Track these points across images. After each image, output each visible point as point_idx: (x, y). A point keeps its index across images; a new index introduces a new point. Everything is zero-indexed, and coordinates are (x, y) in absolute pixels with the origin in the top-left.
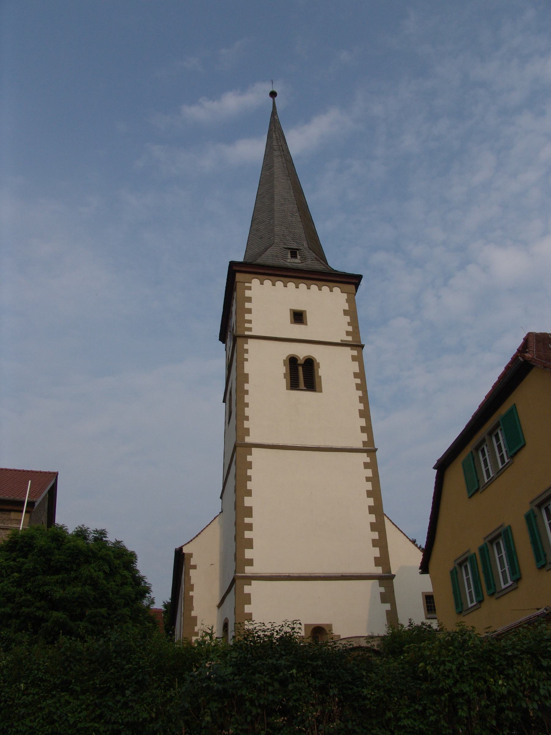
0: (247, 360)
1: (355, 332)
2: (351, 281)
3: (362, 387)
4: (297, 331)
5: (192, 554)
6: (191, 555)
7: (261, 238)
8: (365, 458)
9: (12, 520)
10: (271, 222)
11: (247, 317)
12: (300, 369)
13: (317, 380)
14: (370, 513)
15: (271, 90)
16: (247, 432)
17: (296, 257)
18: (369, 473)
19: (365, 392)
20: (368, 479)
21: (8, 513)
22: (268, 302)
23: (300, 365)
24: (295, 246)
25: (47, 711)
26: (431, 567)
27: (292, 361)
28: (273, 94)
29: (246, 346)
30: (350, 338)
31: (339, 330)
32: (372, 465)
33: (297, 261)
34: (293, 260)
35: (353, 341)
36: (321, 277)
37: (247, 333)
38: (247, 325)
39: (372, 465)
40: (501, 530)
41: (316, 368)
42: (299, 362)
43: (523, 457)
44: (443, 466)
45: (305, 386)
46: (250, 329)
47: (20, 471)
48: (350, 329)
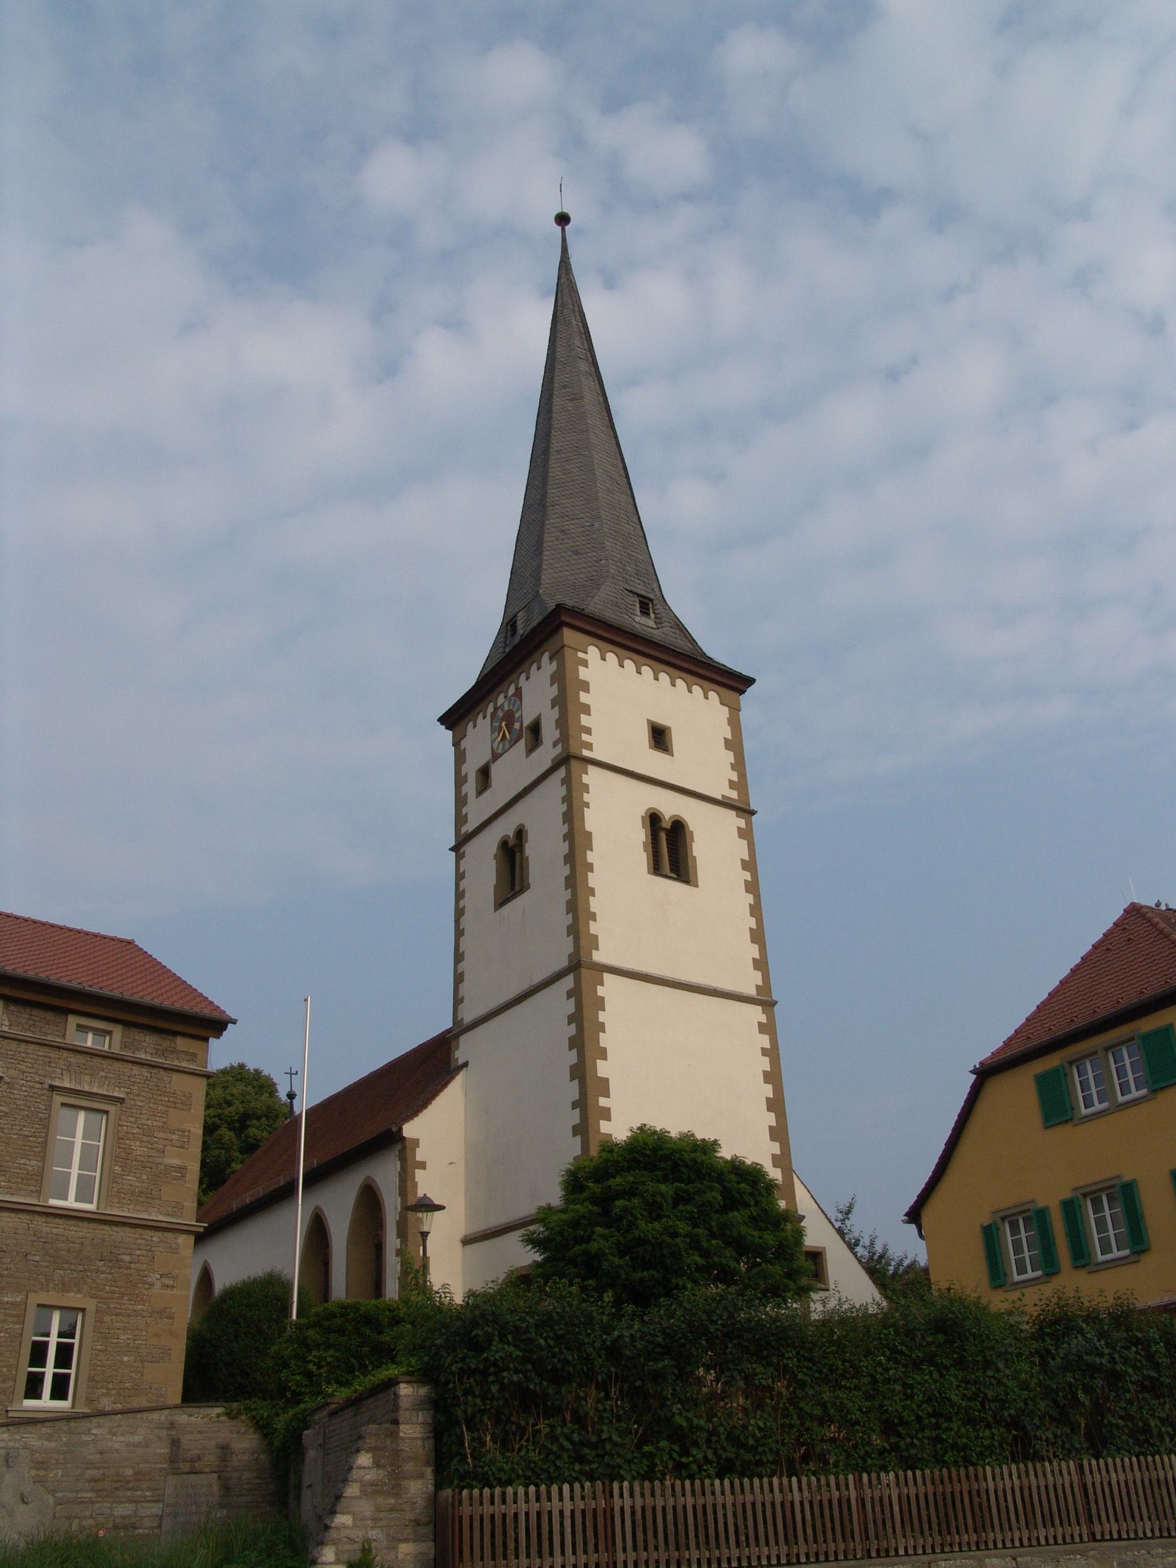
1: (740, 785)
3: (752, 887)
5: (418, 1140)
6: (416, 1143)
7: (577, 553)
8: (756, 1014)
9: (179, 1052)
10: (596, 525)
11: (585, 720)
12: (663, 836)
16: (594, 942)
18: (765, 1041)
19: (757, 897)
20: (765, 1052)
21: (170, 1037)
22: (616, 695)
26: (927, 1216)
27: (654, 819)
29: (586, 779)
30: (734, 795)
31: (716, 777)
34: (644, 620)
36: (719, 678)
37: (586, 753)
38: (585, 737)
39: (768, 1028)
40: (1030, 1206)
44: (986, 1074)
45: (672, 870)
46: (589, 746)
47: (44, 924)
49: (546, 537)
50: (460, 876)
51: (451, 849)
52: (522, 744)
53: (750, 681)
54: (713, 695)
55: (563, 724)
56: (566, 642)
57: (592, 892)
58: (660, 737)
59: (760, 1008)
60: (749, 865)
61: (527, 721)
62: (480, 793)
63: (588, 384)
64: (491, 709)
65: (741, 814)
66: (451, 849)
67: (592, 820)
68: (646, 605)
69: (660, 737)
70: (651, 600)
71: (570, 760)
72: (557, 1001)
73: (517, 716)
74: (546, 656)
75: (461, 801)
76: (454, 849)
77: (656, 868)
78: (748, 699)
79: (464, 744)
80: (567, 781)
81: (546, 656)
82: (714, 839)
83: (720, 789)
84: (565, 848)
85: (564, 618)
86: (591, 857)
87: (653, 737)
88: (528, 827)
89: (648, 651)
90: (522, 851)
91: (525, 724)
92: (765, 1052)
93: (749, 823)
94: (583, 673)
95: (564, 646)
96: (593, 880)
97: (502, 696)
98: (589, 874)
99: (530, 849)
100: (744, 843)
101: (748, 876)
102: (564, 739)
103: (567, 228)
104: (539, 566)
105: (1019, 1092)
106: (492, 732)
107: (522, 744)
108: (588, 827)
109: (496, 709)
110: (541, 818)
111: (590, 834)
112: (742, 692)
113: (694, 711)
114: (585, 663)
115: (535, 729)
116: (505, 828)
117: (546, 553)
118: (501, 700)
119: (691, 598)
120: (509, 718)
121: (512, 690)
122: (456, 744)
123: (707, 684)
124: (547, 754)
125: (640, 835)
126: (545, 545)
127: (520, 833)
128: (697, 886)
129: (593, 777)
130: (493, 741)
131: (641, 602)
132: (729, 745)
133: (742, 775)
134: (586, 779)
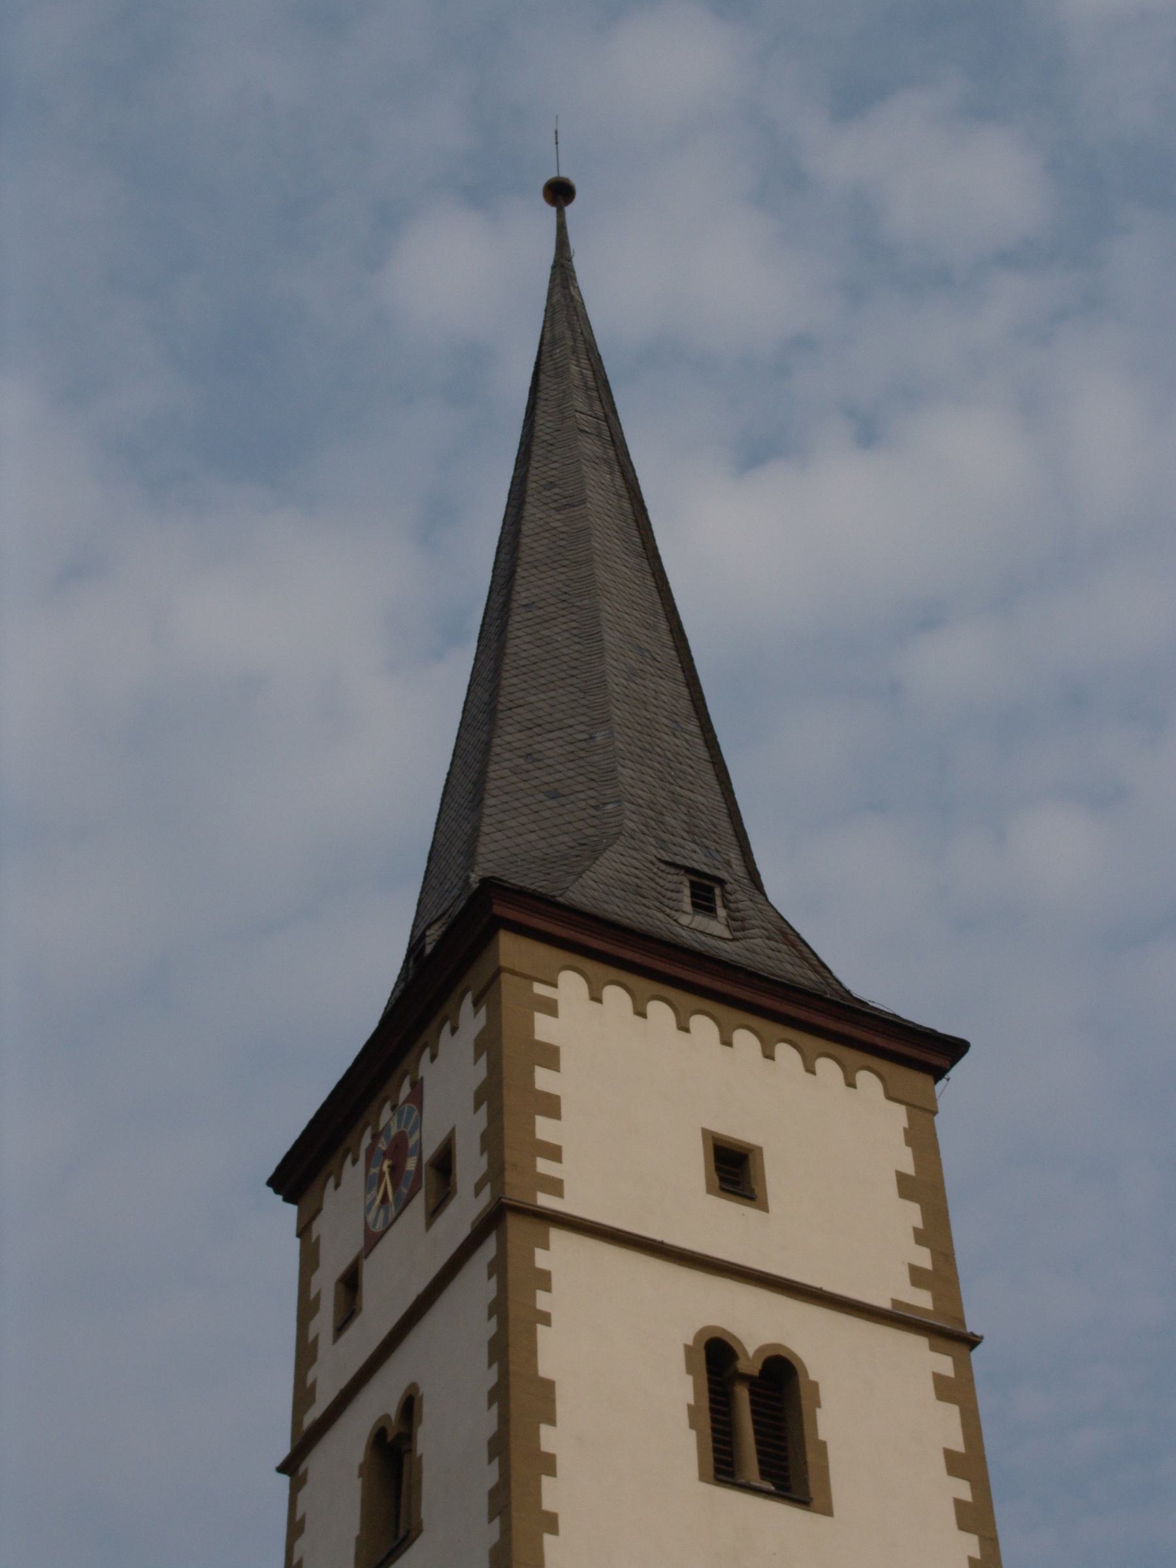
0: (546, 1319)
1: (941, 1276)
2: (917, 1054)
3: (976, 1516)
4: (721, 1227)
7: (554, 795)
10: (600, 737)
12: (743, 1394)
13: (811, 1457)
15: (551, 175)
17: (710, 911)
22: (621, 1081)
24: (699, 862)
27: (716, 1355)
28: (560, 193)
29: (542, 1259)
30: (922, 1299)
31: (884, 1267)
33: (718, 927)
37: (545, 1200)
38: (544, 1166)
41: (805, 1403)
42: (742, 1366)
45: (764, 1475)
46: (555, 1187)
48: (924, 1258)
49: (494, 770)
51: (282, 1469)
52: (418, 1204)
53: (955, 1049)
55: (493, 1141)
56: (504, 962)
57: (551, 1523)
58: (734, 1169)
60: (967, 1463)
61: (429, 1151)
62: (340, 1328)
63: (599, 484)
64: (366, 1141)
65: (940, 1342)
66: (282, 1469)
67: (555, 1354)
68: (705, 892)
69: (734, 1169)
70: (721, 882)
71: (512, 1218)
73: (412, 1142)
74: (468, 1000)
75: (306, 1354)
76: (290, 1466)
77: (723, 1468)
78: (956, 1089)
79: (319, 1227)
80: (498, 1268)
81: (468, 1000)
82: (872, 1405)
83: (889, 1286)
84: (488, 1422)
85: (498, 910)
86: (549, 1439)
87: (718, 1169)
88: (425, 1390)
89: (705, 981)
90: (411, 1450)
93: (964, 1368)
94: (544, 1028)
95: (499, 971)
96: (553, 1494)
97: (388, 1106)
98: (546, 1480)
100: (951, 1414)
101: (963, 1490)
102: (495, 1173)
103: (569, 210)
104: (476, 829)
105: (348, 1195)
106: (368, 1189)
107: (418, 1204)
108: (546, 1367)
109: (375, 1137)
110: (447, 1364)
111: (549, 1386)
112: (939, 1073)
113: (826, 1126)
114: (551, 1008)
115: (444, 1163)
116: (379, 1402)
117: (489, 801)
118: (386, 1115)
119: (837, 890)
120: (399, 1149)
121: (406, 1090)
122: (303, 1231)
123: (852, 1056)
124: (466, 1208)
125: (680, 1390)
126: (489, 786)
127: (410, 1406)
128: (827, 1511)
129: (560, 1254)
130: (368, 1209)
131: (693, 885)
132: (907, 1187)
133: (944, 1255)
134: (542, 1259)
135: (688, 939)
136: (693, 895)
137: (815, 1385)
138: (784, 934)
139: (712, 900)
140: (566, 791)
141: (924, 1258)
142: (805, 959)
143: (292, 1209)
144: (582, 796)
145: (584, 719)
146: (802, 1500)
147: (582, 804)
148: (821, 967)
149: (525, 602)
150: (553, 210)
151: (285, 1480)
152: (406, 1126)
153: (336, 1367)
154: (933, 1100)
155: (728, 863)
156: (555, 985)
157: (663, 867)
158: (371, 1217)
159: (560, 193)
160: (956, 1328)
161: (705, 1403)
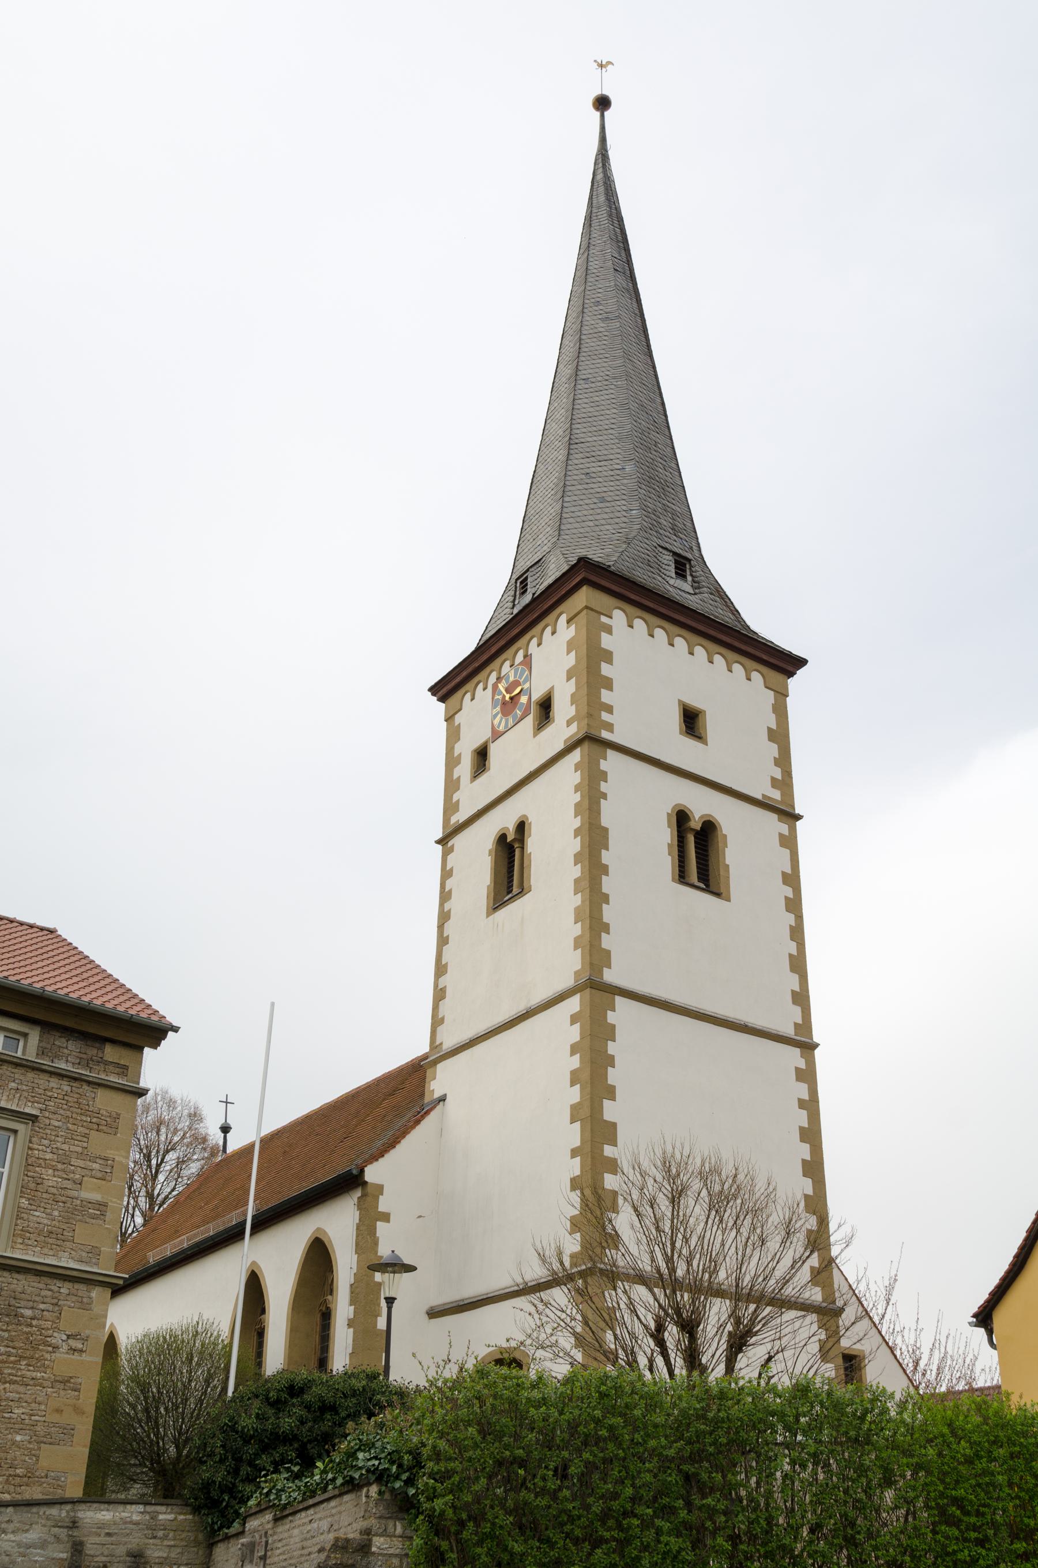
2: (784, 664)
9: (107, 1063)
12: (691, 839)
14: (614, 1125)
15: (597, 92)
20: (802, 1104)
23: (692, 829)
25: (1017, 1449)
27: (681, 817)
28: (602, 103)
30: (776, 795)
32: (807, 1075)
33: (687, 587)
34: (679, 583)
35: (782, 802)
37: (605, 735)
43: (484, 778)
45: (700, 879)
46: (610, 727)
50: (446, 874)
51: (438, 842)
54: (756, 676)
58: (691, 721)
59: (798, 1050)
61: (537, 695)
65: (784, 818)
66: (438, 842)
69: (691, 721)
70: (689, 560)
72: (561, 1028)
74: (563, 618)
75: (451, 785)
77: (682, 877)
78: (794, 684)
81: (563, 618)
87: (685, 721)
89: (682, 619)
91: (533, 699)
92: (802, 1104)
93: (793, 830)
99: (533, 844)
105: (479, 707)
112: (791, 674)
114: (609, 630)
115: (545, 706)
116: (504, 819)
118: (506, 668)
121: (520, 657)
122: (449, 719)
125: (665, 835)
127: (521, 827)
131: (676, 562)
133: (788, 773)
134: (604, 765)
135: (674, 594)
136: (676, 568)
137: (725, 836)
138: (718, 591)
139: (685, 571)
140: (609, 499)
141: (778, 774)
142: (728, 606)
143: (443, 705)
144: (618, 503)
145: (619, 456)
146: (718, 895)
147: (618, 508)
148: (736, 612)
149: (584, 377)
150: (598, 114)
151: (440, 847)
152: (520, 677)
153: (473, 795)
154: (786, 687)
155: (691, 548)
156: (611, 618)
157: (661, 550)
158: (496, 722)
159: (602, 103)
160: (791, 811)
161: (676, 843)
